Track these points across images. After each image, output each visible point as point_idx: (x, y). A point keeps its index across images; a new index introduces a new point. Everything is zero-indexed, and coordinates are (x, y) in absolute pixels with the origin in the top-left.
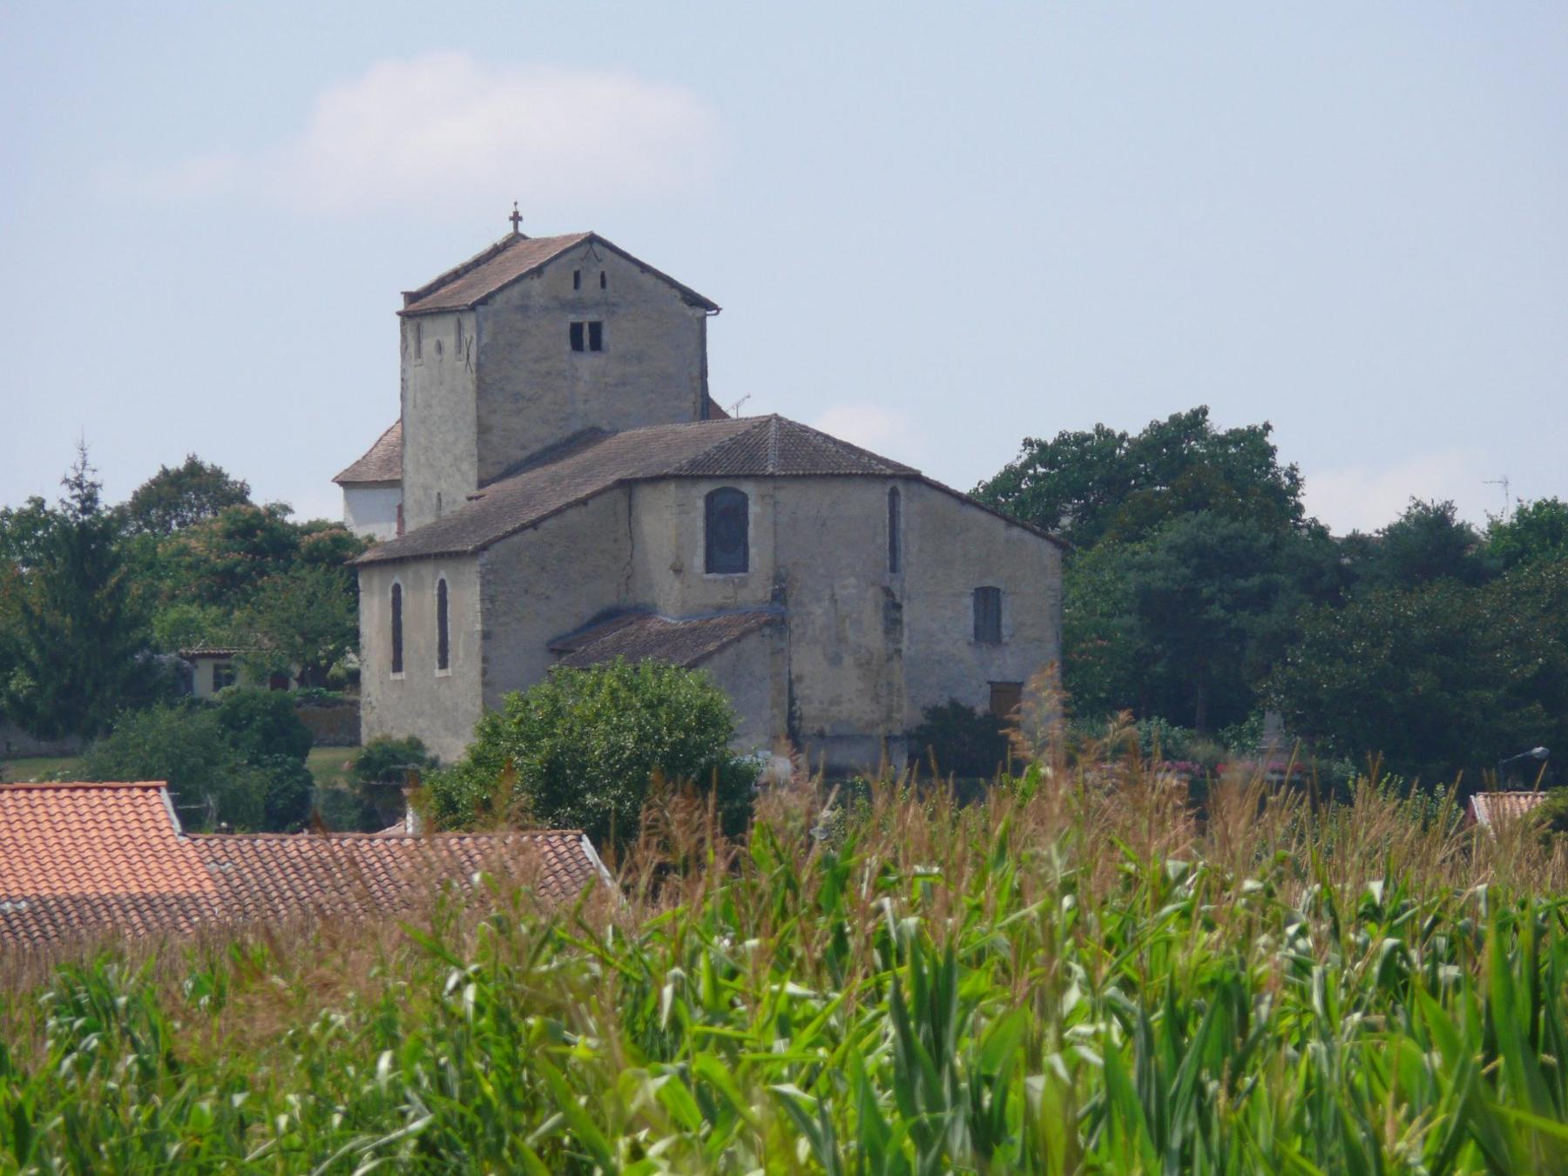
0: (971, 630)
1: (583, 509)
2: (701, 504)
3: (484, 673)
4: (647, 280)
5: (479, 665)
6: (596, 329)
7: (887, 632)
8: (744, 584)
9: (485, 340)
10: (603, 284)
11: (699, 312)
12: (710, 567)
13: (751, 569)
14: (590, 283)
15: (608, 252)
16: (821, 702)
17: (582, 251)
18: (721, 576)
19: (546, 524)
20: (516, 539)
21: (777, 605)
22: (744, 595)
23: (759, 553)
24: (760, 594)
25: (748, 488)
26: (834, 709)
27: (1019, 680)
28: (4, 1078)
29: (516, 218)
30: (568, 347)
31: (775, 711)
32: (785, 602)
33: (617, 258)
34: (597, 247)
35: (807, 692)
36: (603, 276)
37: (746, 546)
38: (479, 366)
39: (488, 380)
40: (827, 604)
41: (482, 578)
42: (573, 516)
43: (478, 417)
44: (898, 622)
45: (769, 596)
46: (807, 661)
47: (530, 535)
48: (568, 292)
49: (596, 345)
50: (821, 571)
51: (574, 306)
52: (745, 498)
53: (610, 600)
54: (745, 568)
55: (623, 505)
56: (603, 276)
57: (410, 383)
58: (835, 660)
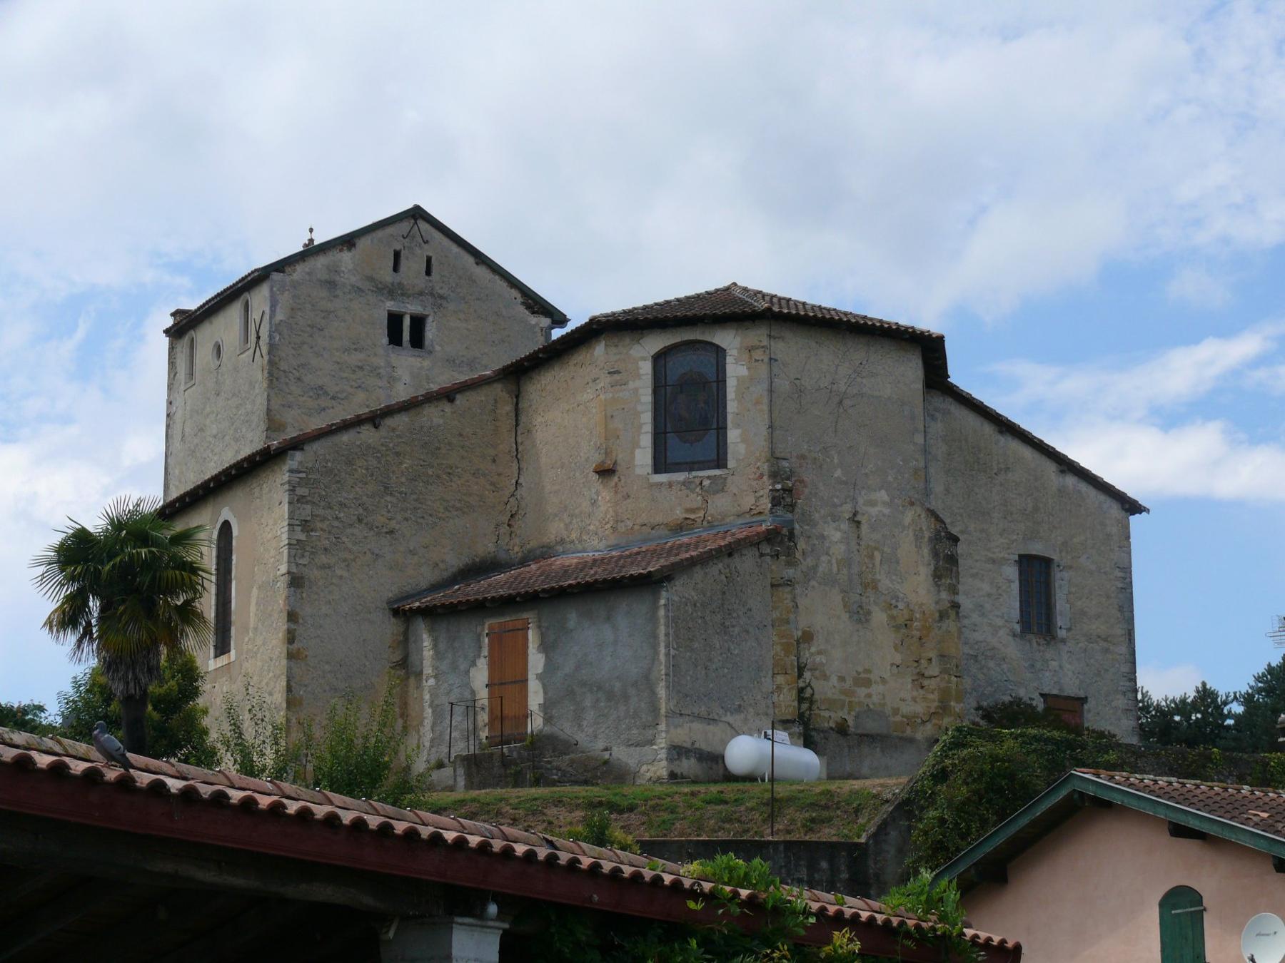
0: (1016, 613)
1: (448, 408)
2: (646, 368)
3: (291, 638)
4: (481, 272)
5: (282, 625)
6: (418, 323)
7: (937, 576)
8: (719, 486)
9: (280, 316)
10: (428, 272)
11: (545, 322)
12: (660, 464)
13: (731, 463)
14: (412, 267)
15: (437, 235)
16: (842, 679)
18: (680, 476)
19: (389, 422)
20: (345, 438)
21: (780, 511)
22: (720, 504)
23: (744, 438)
25: (728, 339)
26: (862, 692)
27: (1082, 694)
29: (311, 230)
30: (385, 340)
31: (780, 679)
32: (791, 507)
33: (446, 242)
34: (423, 226)
35: (818, 659)
36: (429, 260)
37: (722, 429)
38: (272, 347)
39: (283, 366)
40: (845, 526)
41: (292, 490)
42: (434, 415)
43: (269, 410)
44: (952, 560)
45: (766, 504)
46: (820, 610)
47: (367, 434)
48: (387, 276)
49: (418, 341)
50: (838, 473)
51: (392, 291)
52: (720, 352)
53: (486, 547)
54: (720, 462)
56: (429, 260)
57: (178, 417)
58: (860, 615)
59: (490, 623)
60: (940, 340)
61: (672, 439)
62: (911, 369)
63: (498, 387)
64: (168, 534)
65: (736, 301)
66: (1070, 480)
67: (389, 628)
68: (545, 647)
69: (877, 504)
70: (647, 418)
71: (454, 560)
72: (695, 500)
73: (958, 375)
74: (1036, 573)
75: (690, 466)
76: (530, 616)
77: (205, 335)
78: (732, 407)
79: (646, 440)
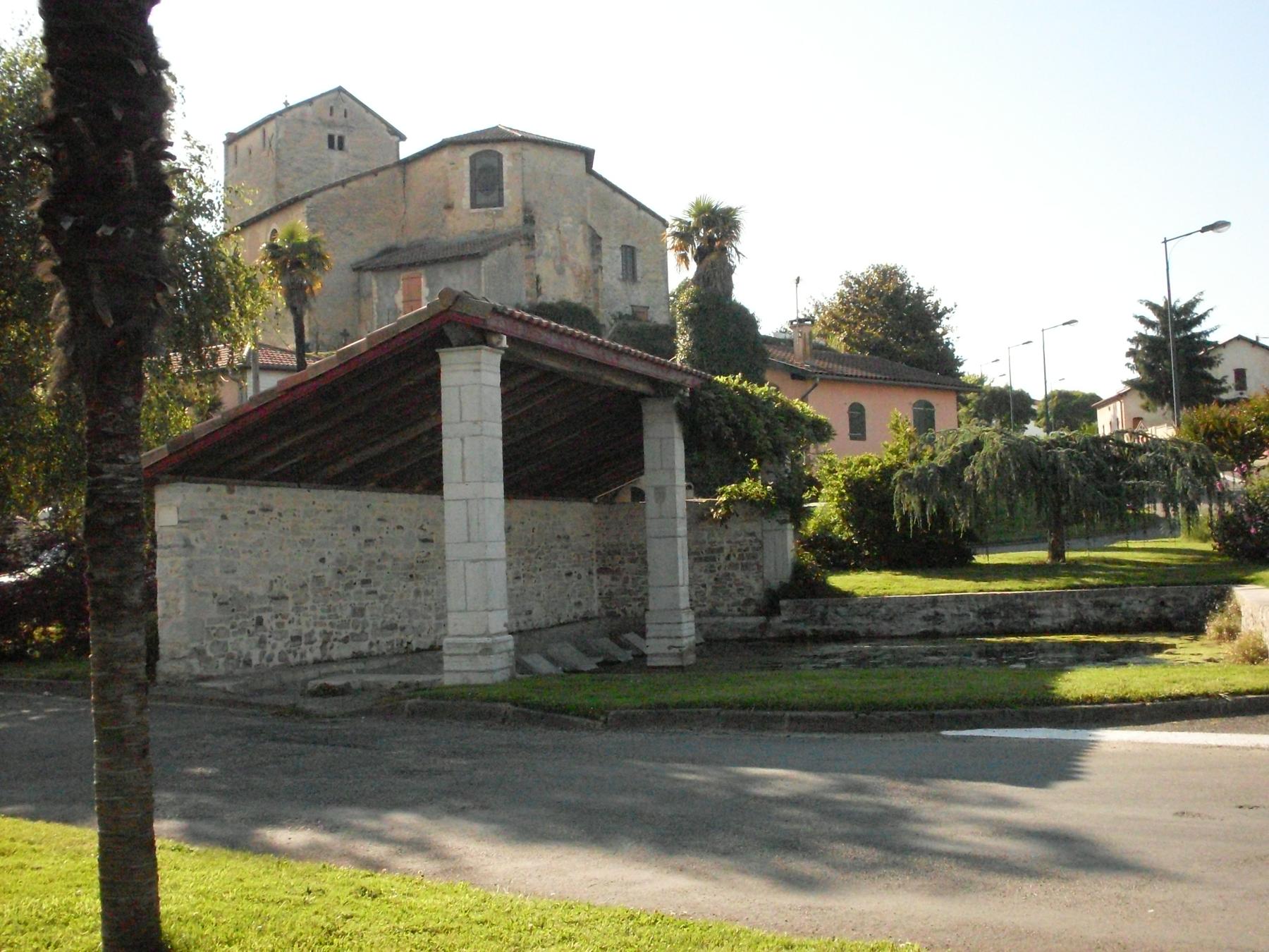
1: (374, 179)
2: (467, 162)
4: (369, 116)
6: (341, 139)
8: (499, 215)
9: (280, 136)
11: (397, 138)
12: (474, 205)
14: (338, 114)
17: (334, 95)
18: (483, 210)
20: (331, 192)
22: (500, 222)
23: (510, 194)
24: (513, 221)
25: (503, 149)
28: (49, 718)
37: (501, 190)
38: (278, 150)
40: (554, 232)
42: (369, 182)
44: (599, 247)
49: (341, 147)
51: (331, 125)
52: (499, 156)
53: (392, 241)
55: (400, 179)
58: (561, 272)
59: (404, 275)
60: (593, 151)
61: (479, 194)
62: (581, 161)
63: (395, 170)
64: (689, 255)
65: (503, 132)
66: (643, 213)
67: (353, 277)
68: (429, 285)
69: (567, 223)
70: (467, 184)
71: (378, 246)
72: (489, 220)
73: (597, 167)
74: (629, 253)
75: (487, 206)
76: (422, 271)
77: (243, 144)
78: (505, 180)
79: (467, 193)
